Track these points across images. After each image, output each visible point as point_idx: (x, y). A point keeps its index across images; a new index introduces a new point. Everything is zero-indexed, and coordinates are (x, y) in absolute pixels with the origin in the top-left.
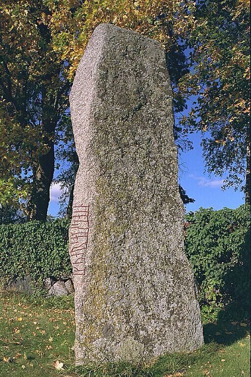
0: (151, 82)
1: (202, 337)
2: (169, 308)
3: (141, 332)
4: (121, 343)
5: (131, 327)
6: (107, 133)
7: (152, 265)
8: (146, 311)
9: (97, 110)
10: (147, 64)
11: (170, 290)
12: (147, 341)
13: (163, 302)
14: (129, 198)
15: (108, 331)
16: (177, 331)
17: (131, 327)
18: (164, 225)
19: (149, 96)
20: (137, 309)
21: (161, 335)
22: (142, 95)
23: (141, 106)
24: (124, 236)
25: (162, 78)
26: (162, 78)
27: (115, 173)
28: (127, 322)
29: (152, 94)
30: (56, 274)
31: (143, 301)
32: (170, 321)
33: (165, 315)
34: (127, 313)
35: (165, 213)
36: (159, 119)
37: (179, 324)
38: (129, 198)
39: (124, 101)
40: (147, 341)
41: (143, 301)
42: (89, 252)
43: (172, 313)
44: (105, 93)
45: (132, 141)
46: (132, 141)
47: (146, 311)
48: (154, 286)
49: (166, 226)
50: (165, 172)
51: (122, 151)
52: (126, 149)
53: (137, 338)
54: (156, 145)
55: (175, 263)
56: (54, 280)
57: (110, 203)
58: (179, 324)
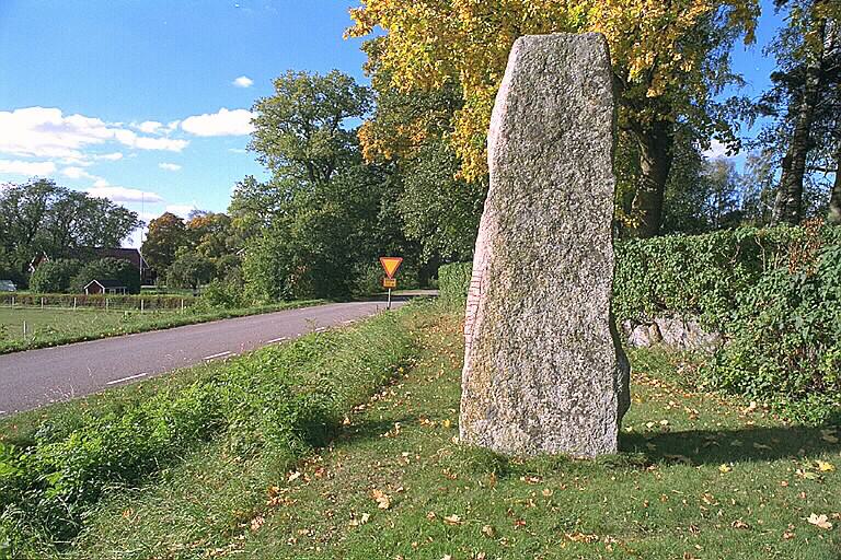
0: (579, 97)
1: (615, 441)
2: (570, 397)
3: (530, 421)
4: (503, 429)
5: (517, 413)
6: (511, 179)
7: (556, 341)
8: (540, 396)
9: (502, 153)
10: (575, 71)
11: (576, 375)
12: (536, 433)
13: (563, 388)
14: (535, 257)
15: (491, 413)
16: (576, 428)
17: (517, 413)
18: (579, 289)
19: (576, 117)
20: (528, 394)
21: (555, 429)
22: (565, 118)
23: (563, 132)
24: (522, 305)
25: (597, 85)
26: (597, 85)
27: (518, 227)
28: (514, 407)
29: (579, 112)
30: (638, 314)
31: (537, 385)
32: (569, 413)
33: (564, 405)
34: (516, 396)
35: (583, 273)
36: (589, 144)
37: (581, 419)
38: (535, 257)
39: (537, 133)
40: (536, 433)
41: (537, 385)
42: (479, 322)
43: (574, 403)
44: (514, 128)
45: (546, 183)
46: (546, 183)
47: (540, 396)
48: (554, 367)
49: (582, 291)
50: (592, 216)
51: (531, 199)
52: (537, 195)
53: (523, 425)
54: (581, 181)
55: (590, 339)
56: (636, 322)
57: (507, 266)
58: (581, 419)
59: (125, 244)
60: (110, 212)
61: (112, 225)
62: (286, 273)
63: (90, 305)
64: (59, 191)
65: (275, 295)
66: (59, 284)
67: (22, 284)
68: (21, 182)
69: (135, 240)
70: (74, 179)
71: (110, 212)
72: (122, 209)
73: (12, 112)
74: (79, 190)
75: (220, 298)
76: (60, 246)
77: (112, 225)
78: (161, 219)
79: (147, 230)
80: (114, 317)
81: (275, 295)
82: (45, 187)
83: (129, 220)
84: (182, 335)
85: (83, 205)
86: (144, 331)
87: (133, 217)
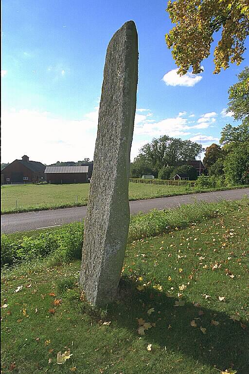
59: (197, 159)
60: (191, 146)
61: (192, 150)
62: (242, 171)
63: (174, 185)
64: (170, 139)
65: (236, 181)
66: (167, 176)
67: (156, 177)
68: (158, 137)
69: (201, 157)
70: (174, 135)
71: (191, 146)
72: (196, 144)
73: (25, 158)
74: (177, 138)
75: (205, 184)
76: (172, 161)
77: (192, 150)
78: (211, 147)
79: (205, 152)
80: (182, 189)
81: (236, 181)
82: (165, 138)
83: (196, 148)
84: (171, 199)
85: (177, 143)
86: (158, 198)
87: (200, 146)
